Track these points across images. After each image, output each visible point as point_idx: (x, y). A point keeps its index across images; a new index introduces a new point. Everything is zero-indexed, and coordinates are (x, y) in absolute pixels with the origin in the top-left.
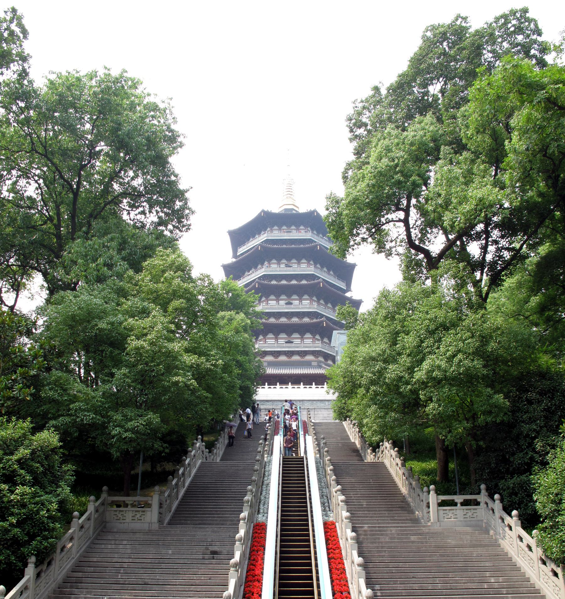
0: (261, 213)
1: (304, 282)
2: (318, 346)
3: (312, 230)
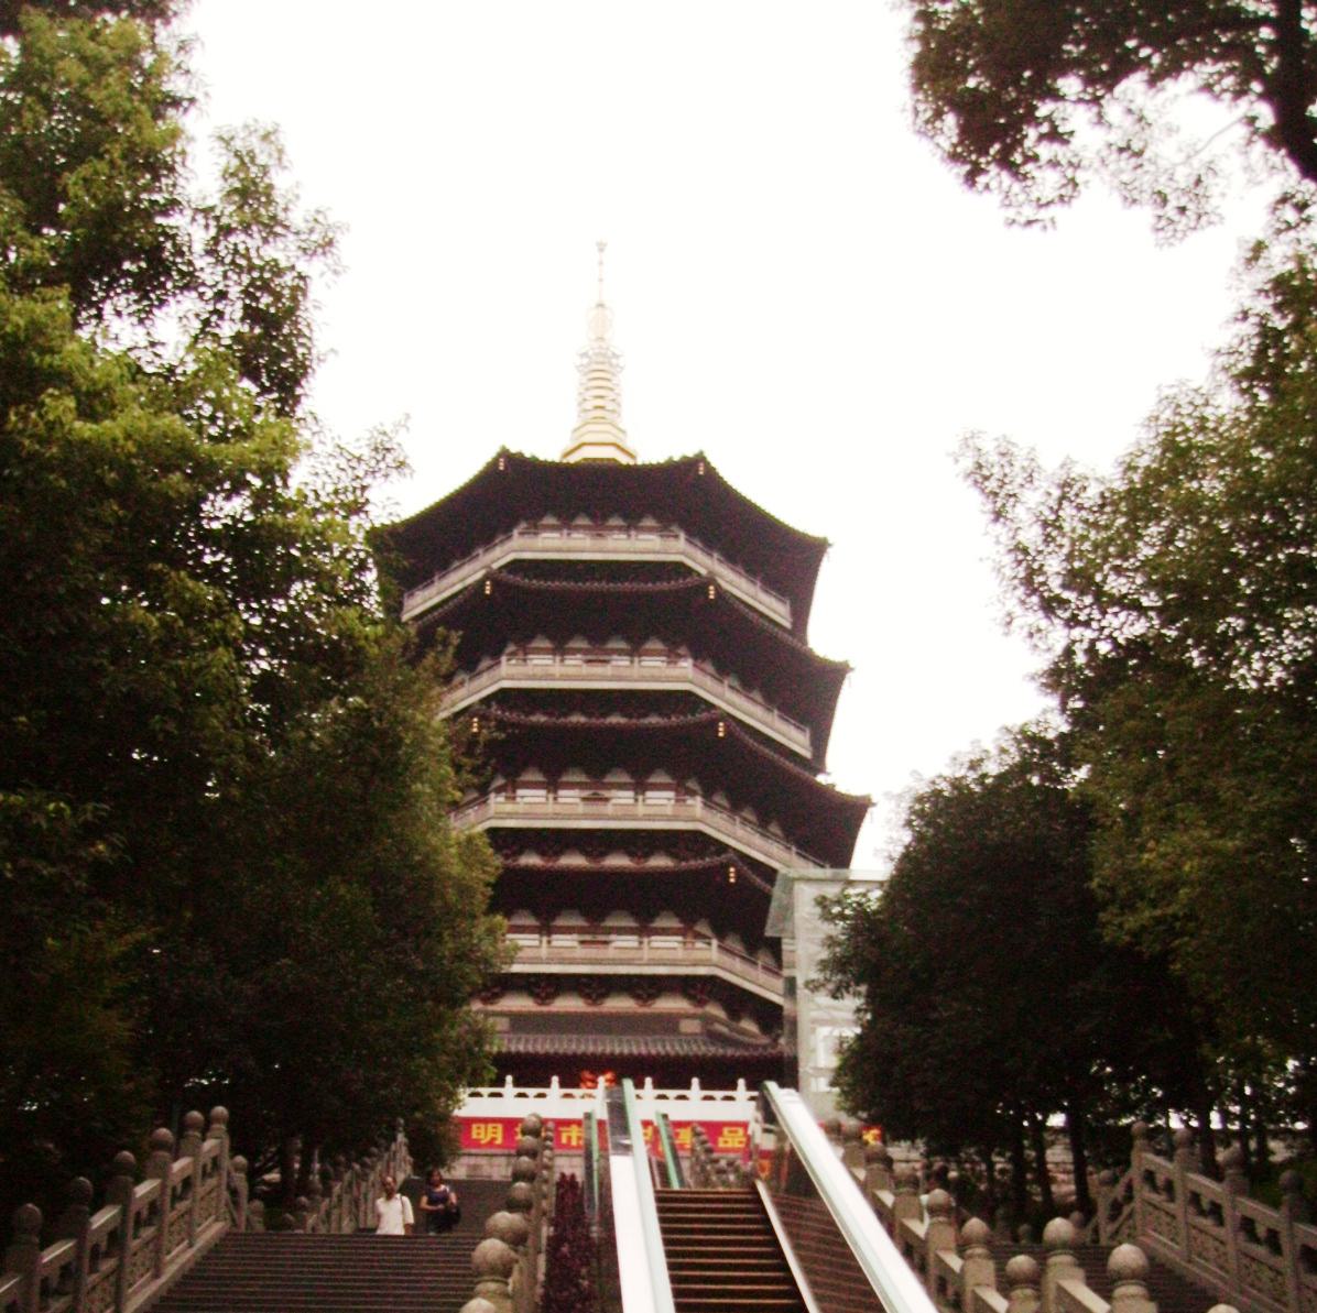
0: (495, 462)
1: (660, 862)
2: (707, 957)
3: (721, 934)
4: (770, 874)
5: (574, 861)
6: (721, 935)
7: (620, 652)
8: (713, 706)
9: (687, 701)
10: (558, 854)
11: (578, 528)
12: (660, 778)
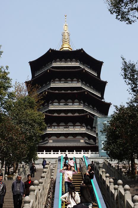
2: (83, 130)
4: (94, 115)
5: (63, 114)
6: (87, 126)
7: (70, 81)
8: (85, 89)
9: (80, 88)
10: (60, 114)
11: (62, 61)
12: (76, 101)
